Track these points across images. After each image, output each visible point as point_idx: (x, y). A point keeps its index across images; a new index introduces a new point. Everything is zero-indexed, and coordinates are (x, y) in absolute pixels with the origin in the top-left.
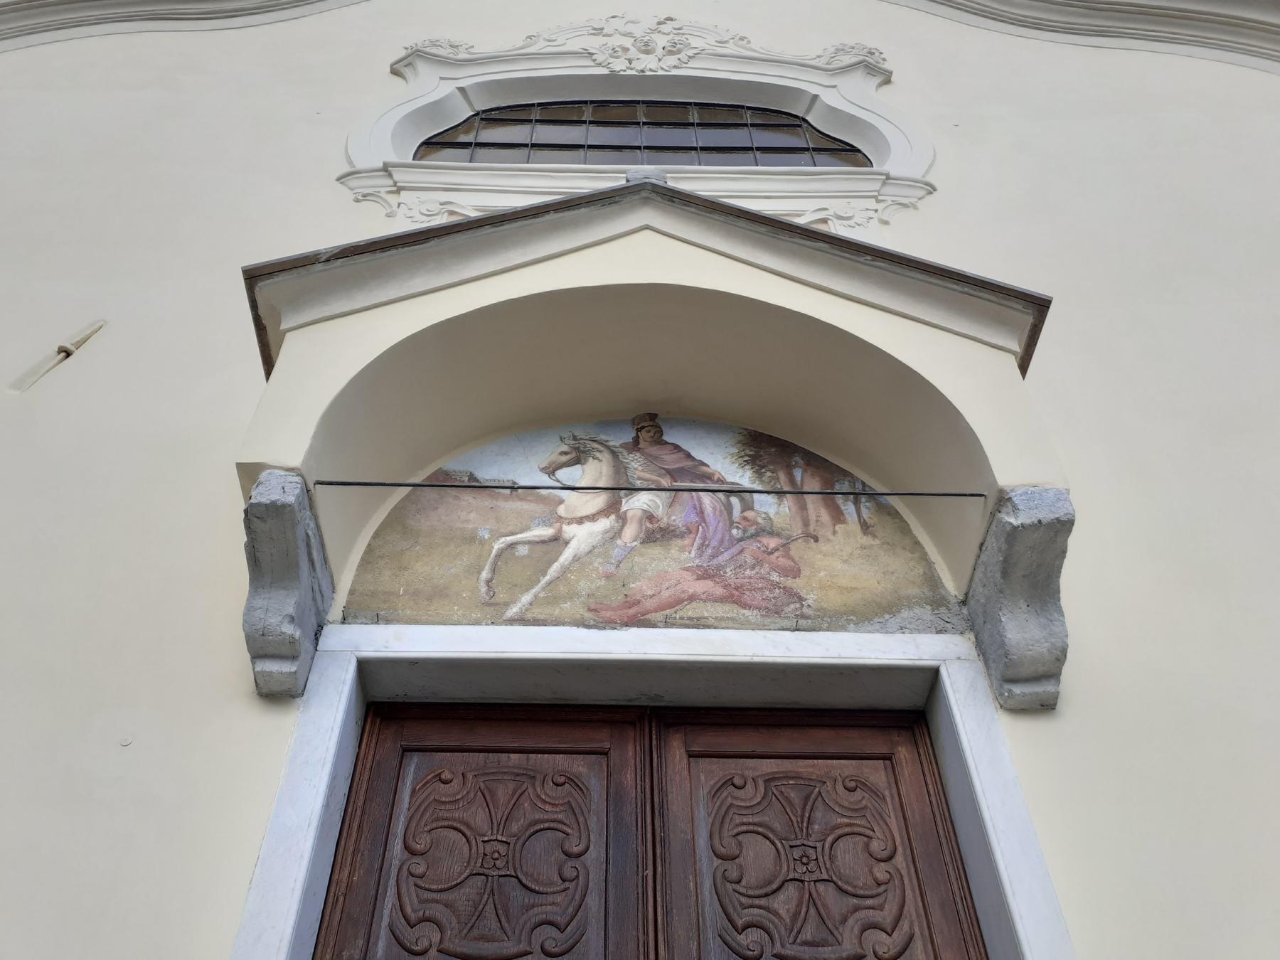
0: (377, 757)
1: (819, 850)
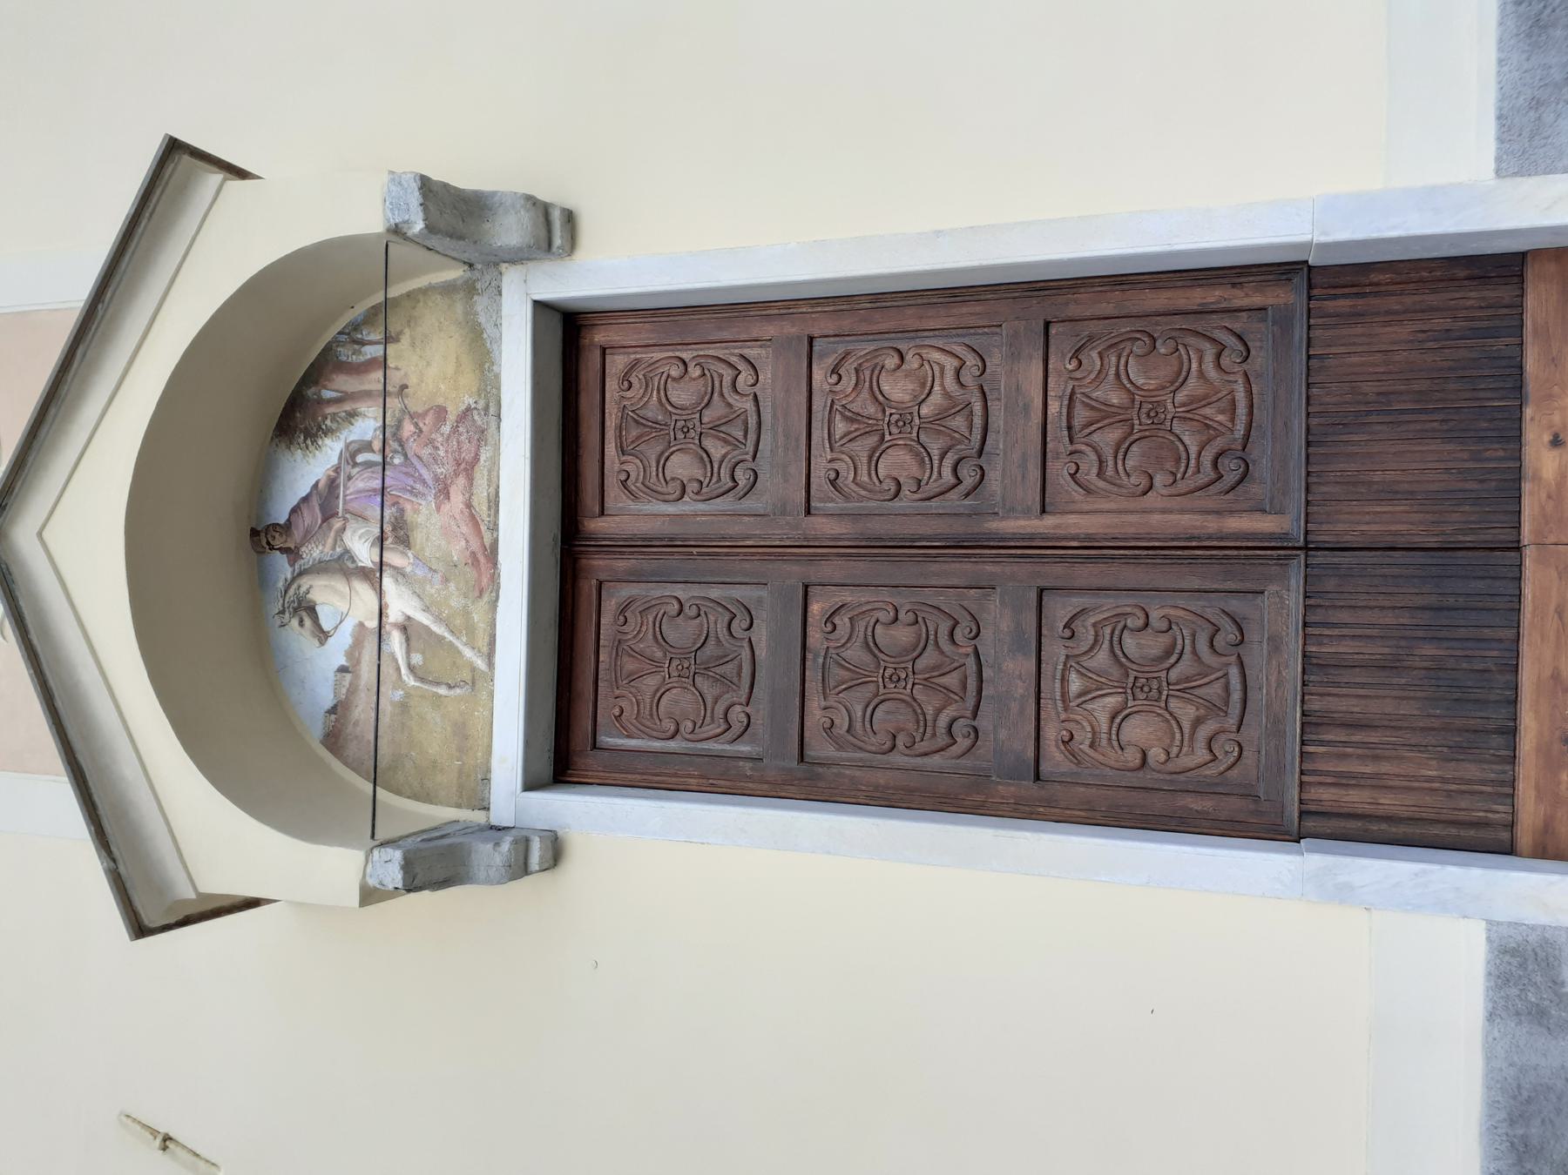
0: (600, 768)
1: (678, 417)
